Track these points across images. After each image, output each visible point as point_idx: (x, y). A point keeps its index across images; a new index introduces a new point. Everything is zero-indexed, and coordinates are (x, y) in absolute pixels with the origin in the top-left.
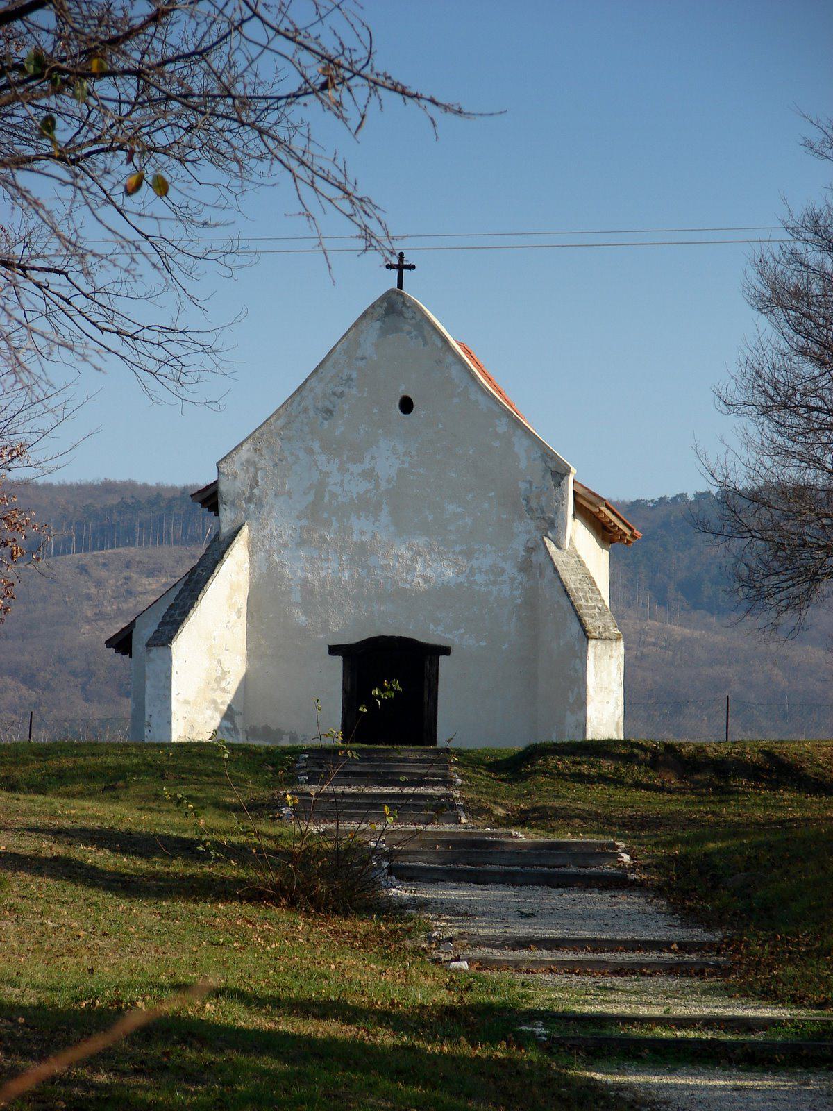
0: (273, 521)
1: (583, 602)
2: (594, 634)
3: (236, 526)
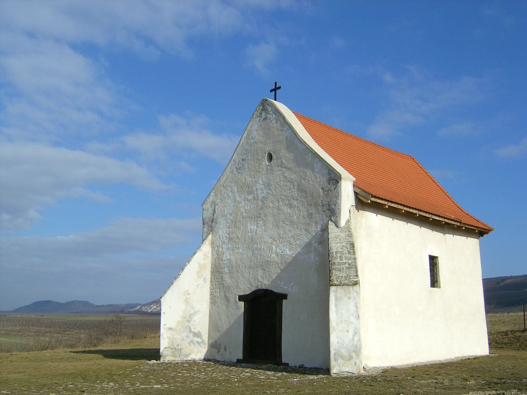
2: (335, 282)
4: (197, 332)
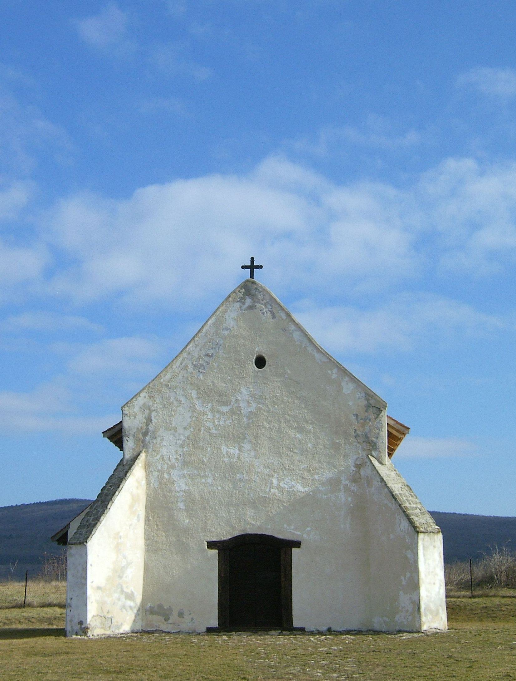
0: (164, 448)
1: (407, 505)
2: (422, 529)
3: (138, 451)
4: (130, 592)
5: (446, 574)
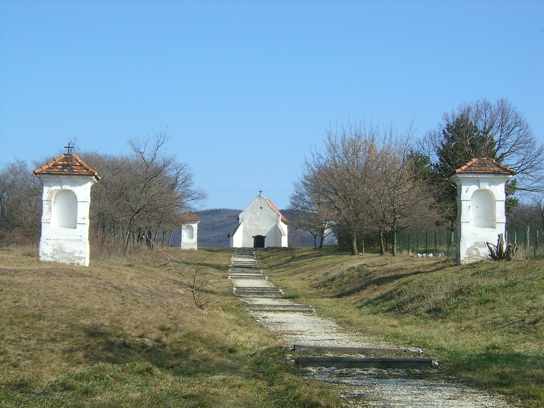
5: (460, 196)
